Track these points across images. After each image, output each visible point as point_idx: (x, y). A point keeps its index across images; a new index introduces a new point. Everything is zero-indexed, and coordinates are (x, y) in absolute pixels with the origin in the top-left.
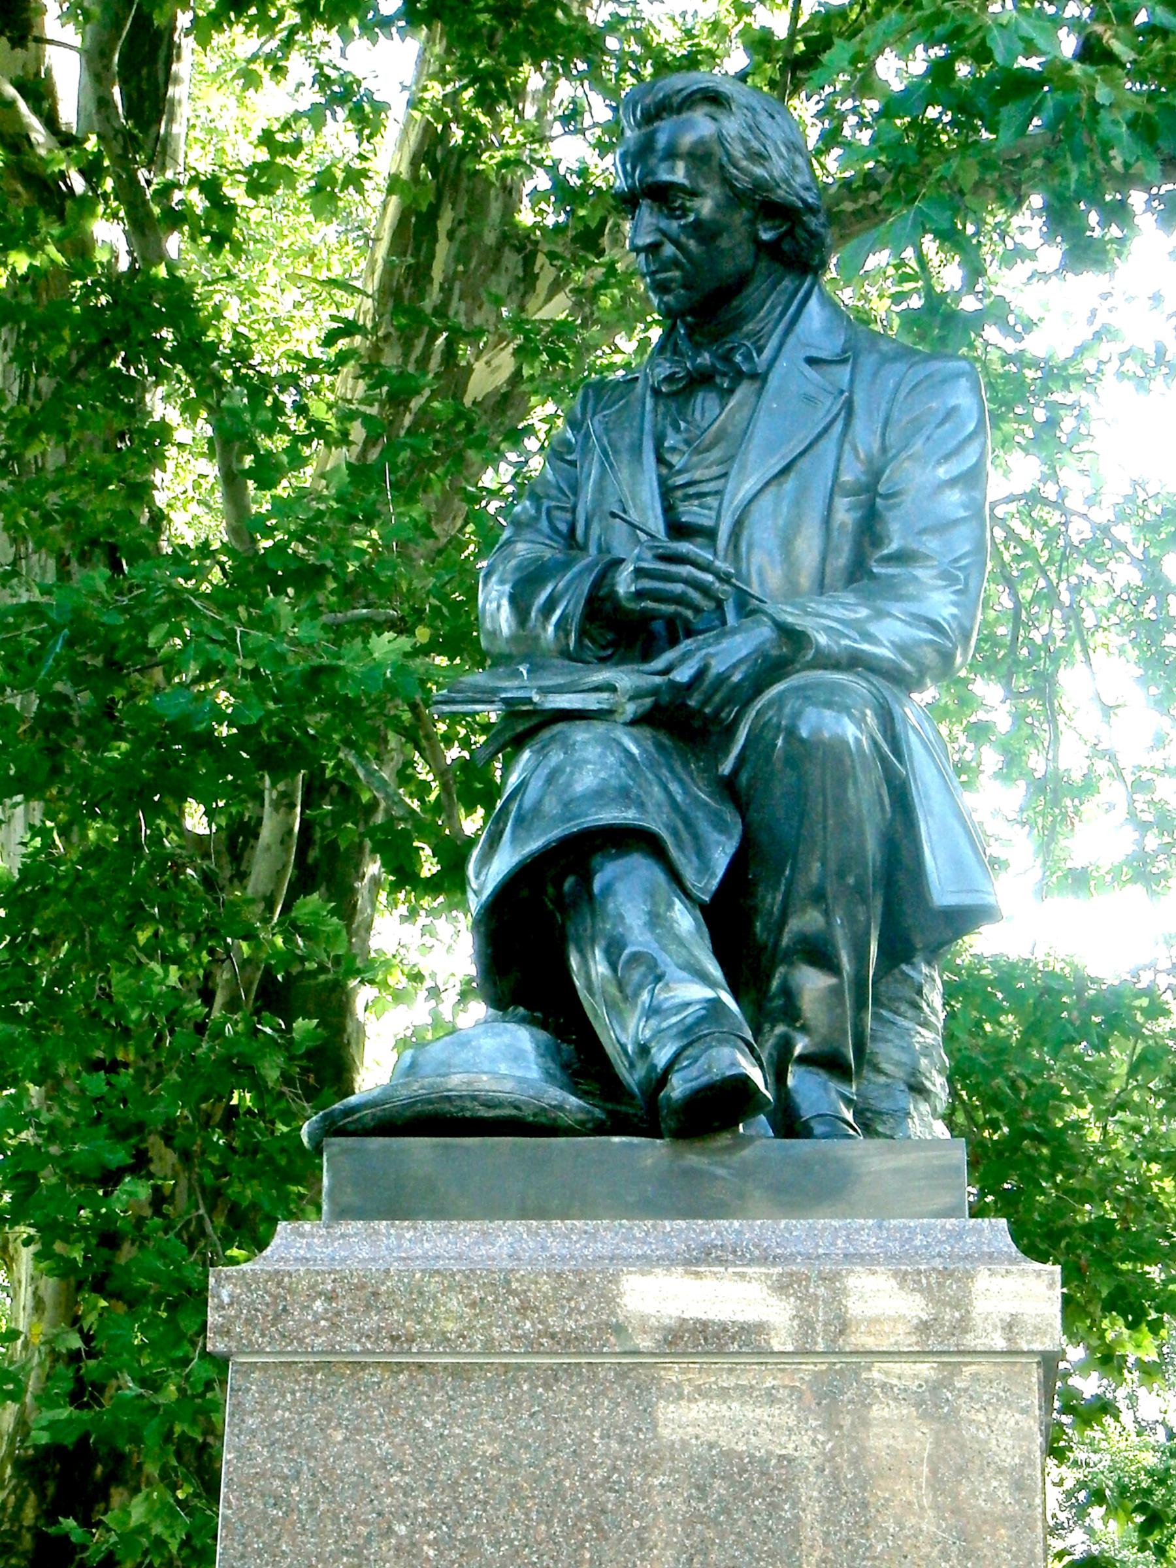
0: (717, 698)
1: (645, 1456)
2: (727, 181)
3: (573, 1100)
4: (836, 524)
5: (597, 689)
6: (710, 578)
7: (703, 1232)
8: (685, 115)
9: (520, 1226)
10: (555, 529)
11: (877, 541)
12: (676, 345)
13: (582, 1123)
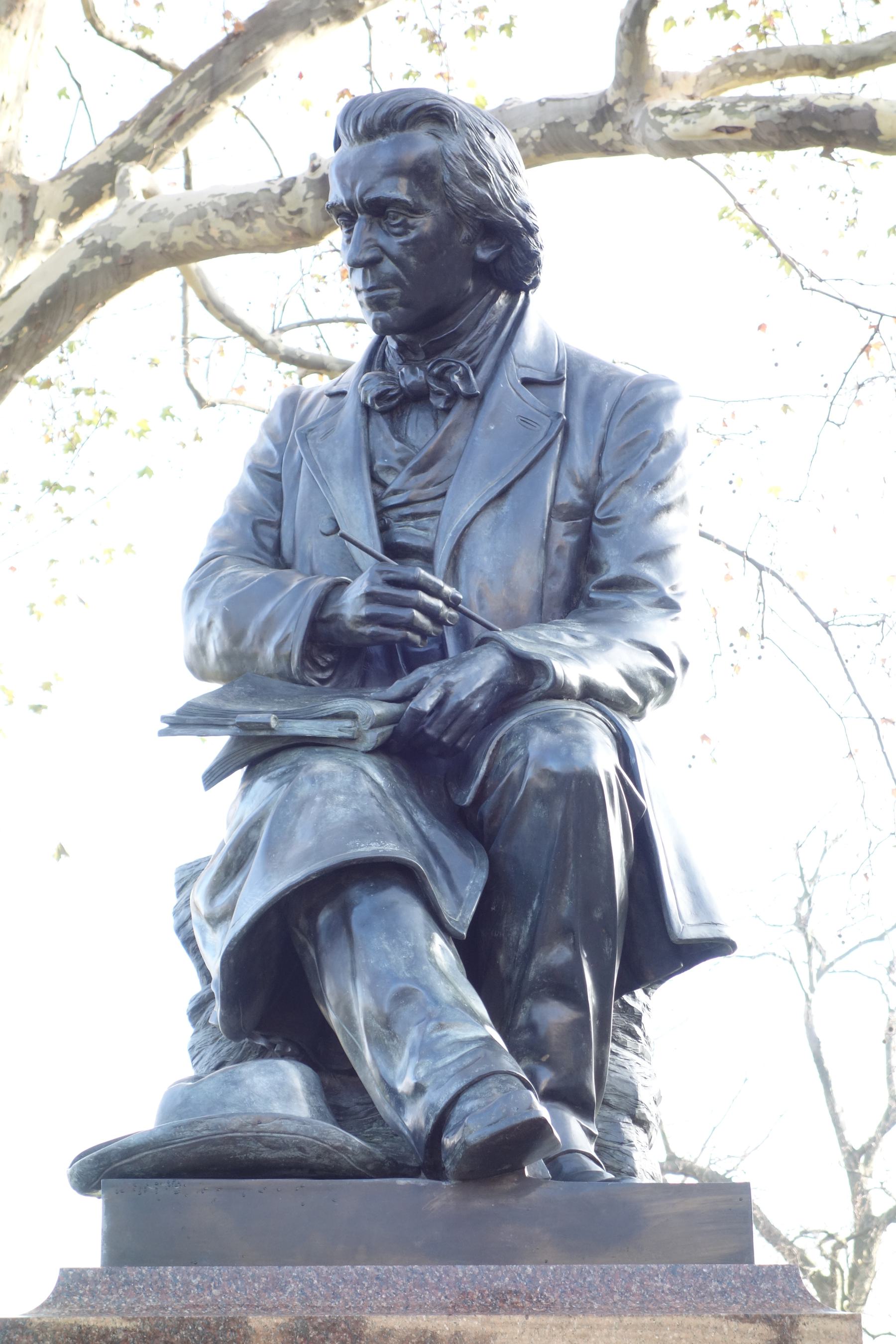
0: (456, 727)
2: (447, 199)
4: (554, 547)
5: (337, 716)
6: (439, 603)
7: (497, 1278)
8: (406, 133)
9: (310, 1272)
10: (263, 546)
11: (594, 567)
12: (384, 358)
13: (363, 1164)
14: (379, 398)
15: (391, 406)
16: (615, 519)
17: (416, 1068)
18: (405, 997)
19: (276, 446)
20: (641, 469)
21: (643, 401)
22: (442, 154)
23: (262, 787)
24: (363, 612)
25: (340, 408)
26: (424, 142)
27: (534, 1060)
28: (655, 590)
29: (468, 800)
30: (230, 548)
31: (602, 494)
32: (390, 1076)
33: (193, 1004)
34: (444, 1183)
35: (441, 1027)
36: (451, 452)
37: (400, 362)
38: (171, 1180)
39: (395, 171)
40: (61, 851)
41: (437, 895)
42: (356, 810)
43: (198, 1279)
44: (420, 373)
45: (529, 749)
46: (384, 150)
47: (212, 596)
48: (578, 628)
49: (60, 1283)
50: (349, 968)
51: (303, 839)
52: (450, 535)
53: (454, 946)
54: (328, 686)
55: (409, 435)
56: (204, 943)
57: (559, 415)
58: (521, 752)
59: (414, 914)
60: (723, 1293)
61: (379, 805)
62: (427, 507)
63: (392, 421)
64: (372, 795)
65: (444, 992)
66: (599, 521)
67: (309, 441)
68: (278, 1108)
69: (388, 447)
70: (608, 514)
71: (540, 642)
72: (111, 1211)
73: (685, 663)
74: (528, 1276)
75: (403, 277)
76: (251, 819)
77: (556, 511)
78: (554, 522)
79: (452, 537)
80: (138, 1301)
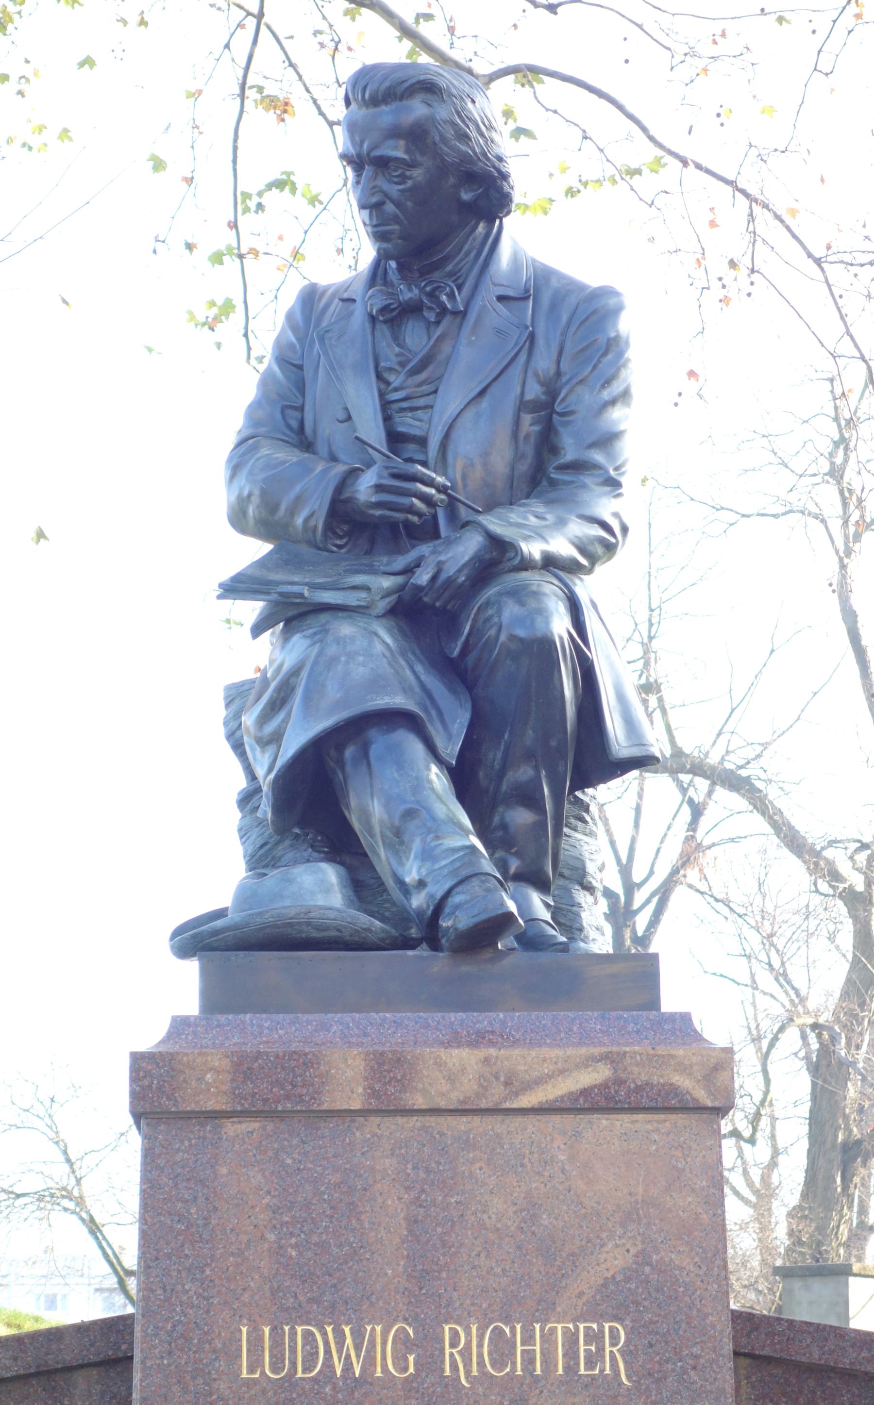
0: (447, 595)
1: (444, 1182)
2: (437, 154)
3: (377, 923)
4: (522, 435)
5: (355, 588)
6: (433, 491)
7: (478, 1022)
8: (405, 102)
9: (347, 1017)
11: (555, 450)
13: (383, 940)
14: (384, 310)
15: (393, 317)
16: (572, 413)
17: (419, 869)
18: (412, 813)
19: (298, 339)
20: (592, 371)
21: (594, 312)
22: (432, 119)
23: (299, 643)
24: (373, 499)
25: (351, 314)
26: (418, 109)
27: (506, 851)
28: (601, 472)
29: (456, 653)
30: (263, 430)
31: (560, 392)
32: (400, 872)
33: (241, 796)
34: (441, 954)
35: (437, 838)
36: (441, 357)
37: (399, 277)
38: (246, 953)
39: (395, 133)
40: (41, 535)
41: (433, 733)
42: (372, 669)
43: (269, 1023)
44: (416, 291)
45: (503, 618)
46: (386, 115)
47: (251, 473)
48: (541, 509)
49: (171, 1026)
50: (369, 790)
51: (332, 691)
52: (440, 428)
53: (446, 772)
54: (343, 551)
55: (407, 341)
56: (255, 759)
57: (527, 327)
58: (496, 620)
59: (417, 748)
60: (638, 1032)
61: (390, 664)
62: (421, 402)
63: (393, 329)
64: (384, 656)
65: (440, 811)
66: (559, 414)
67: (326, 341)
68: (321, 900)
69: (390, 353)
70: (565, 408)
71: (511, 524)
72: (205, 974)
73: (625, 529)
74: (500, 1020)
75: (402, 217)
76: (291, 669)
77: (523, 406)
78: (522, 415)
79: (442, 430)
80: (227, 1038)
